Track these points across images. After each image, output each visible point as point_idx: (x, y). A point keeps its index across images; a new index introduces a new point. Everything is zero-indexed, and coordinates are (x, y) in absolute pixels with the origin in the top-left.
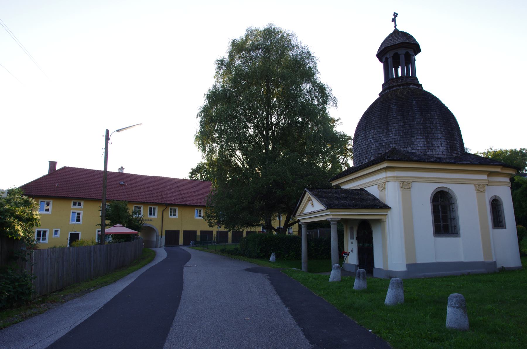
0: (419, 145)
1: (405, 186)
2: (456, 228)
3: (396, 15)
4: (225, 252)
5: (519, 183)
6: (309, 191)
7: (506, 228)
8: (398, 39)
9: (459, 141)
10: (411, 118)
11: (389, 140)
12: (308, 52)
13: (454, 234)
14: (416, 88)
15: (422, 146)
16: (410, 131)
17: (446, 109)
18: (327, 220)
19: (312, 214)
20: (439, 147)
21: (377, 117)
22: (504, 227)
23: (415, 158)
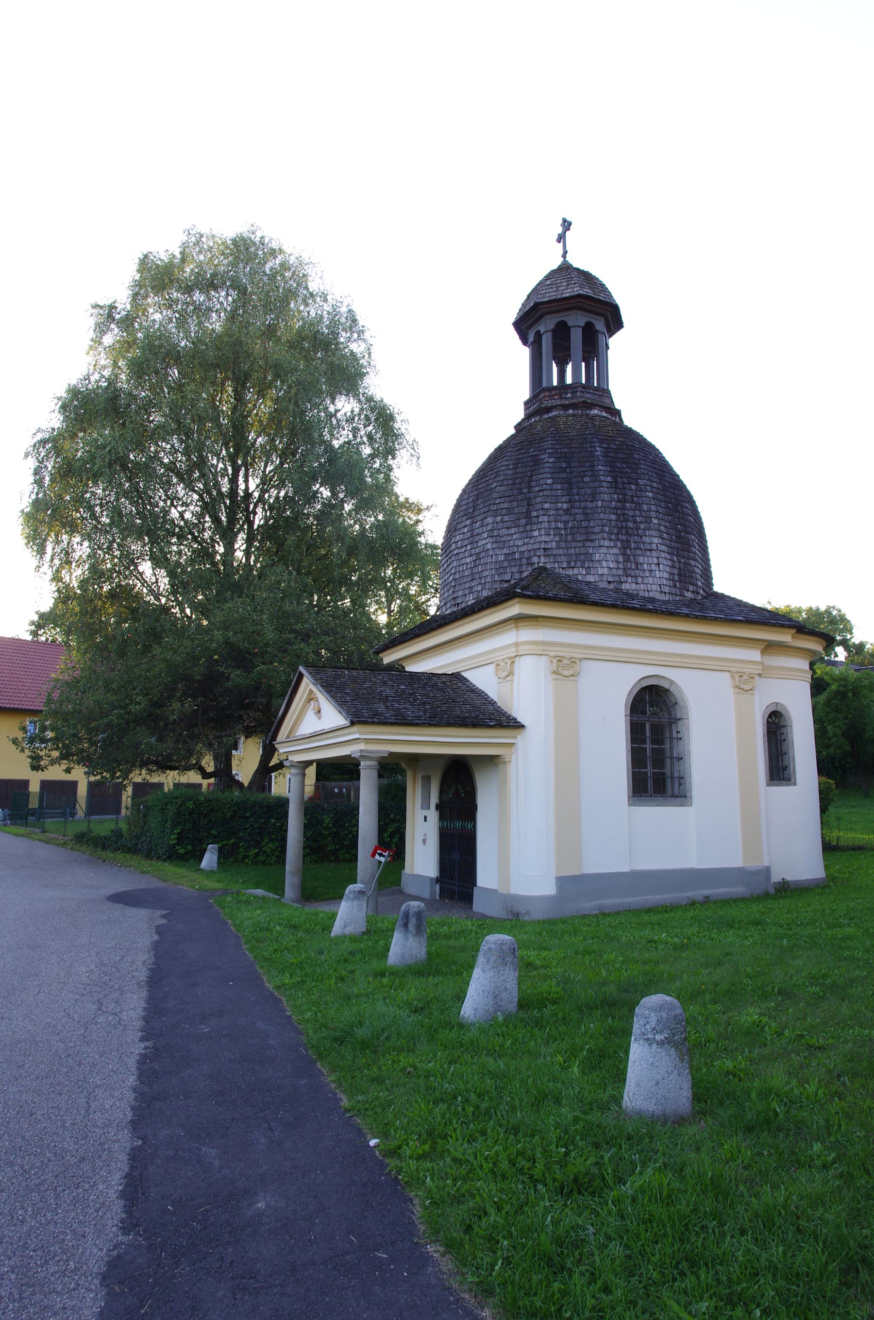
0: (604, 564)
2: (682, 781)
3: (567, 225)
4: (88, 840)
5: (823, 679)
6: (310, 674)
7: (795, 784)
8: (568, 285)
9: (700, 561)
10: (588, 491)
11: (529, 545)
12: (350, 311)
13: (677, 797)
14: (607, 417)
15: (611, 566)
16: (584, 524)
17: (675, 477)
18: (353, 756)
19: (313, 739)
20: (653, 573)
21: (505, 482)
22: (793, 781)
23: (593, 597)
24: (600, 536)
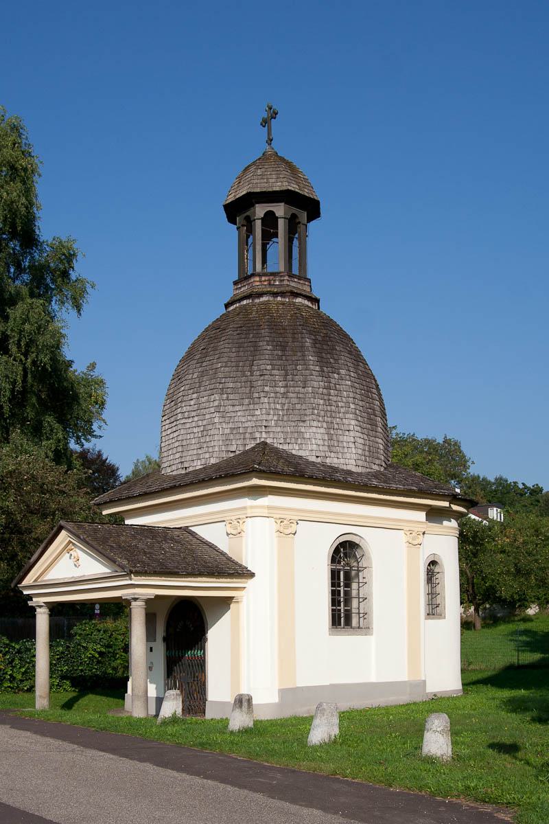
0: (313, 441)
1: (287, 527)
7: (445, 618)
16: (298, 407)
18: (123, 598)
22: (443, 615)
24: (311, 418)
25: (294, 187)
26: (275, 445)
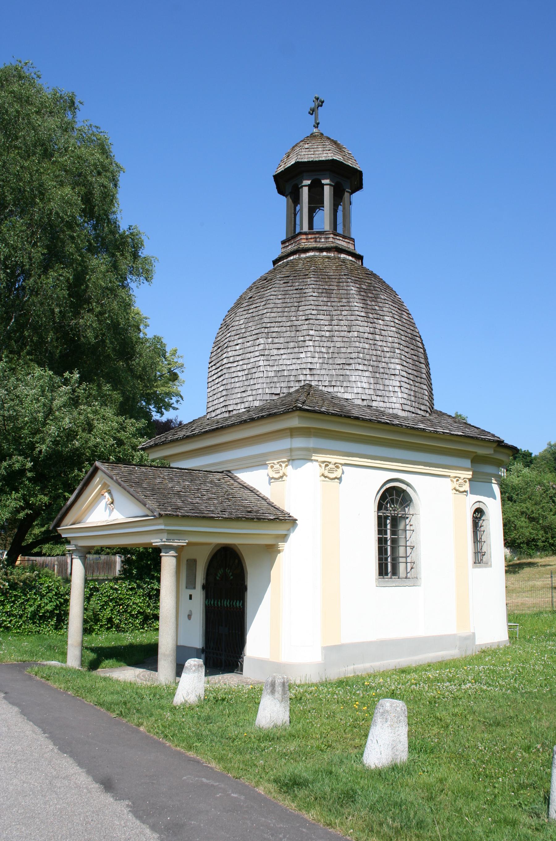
7: (491, 566)
22: (489, 563)
24: (356, 361)
25: (338, 157)
26: (320, 388)
